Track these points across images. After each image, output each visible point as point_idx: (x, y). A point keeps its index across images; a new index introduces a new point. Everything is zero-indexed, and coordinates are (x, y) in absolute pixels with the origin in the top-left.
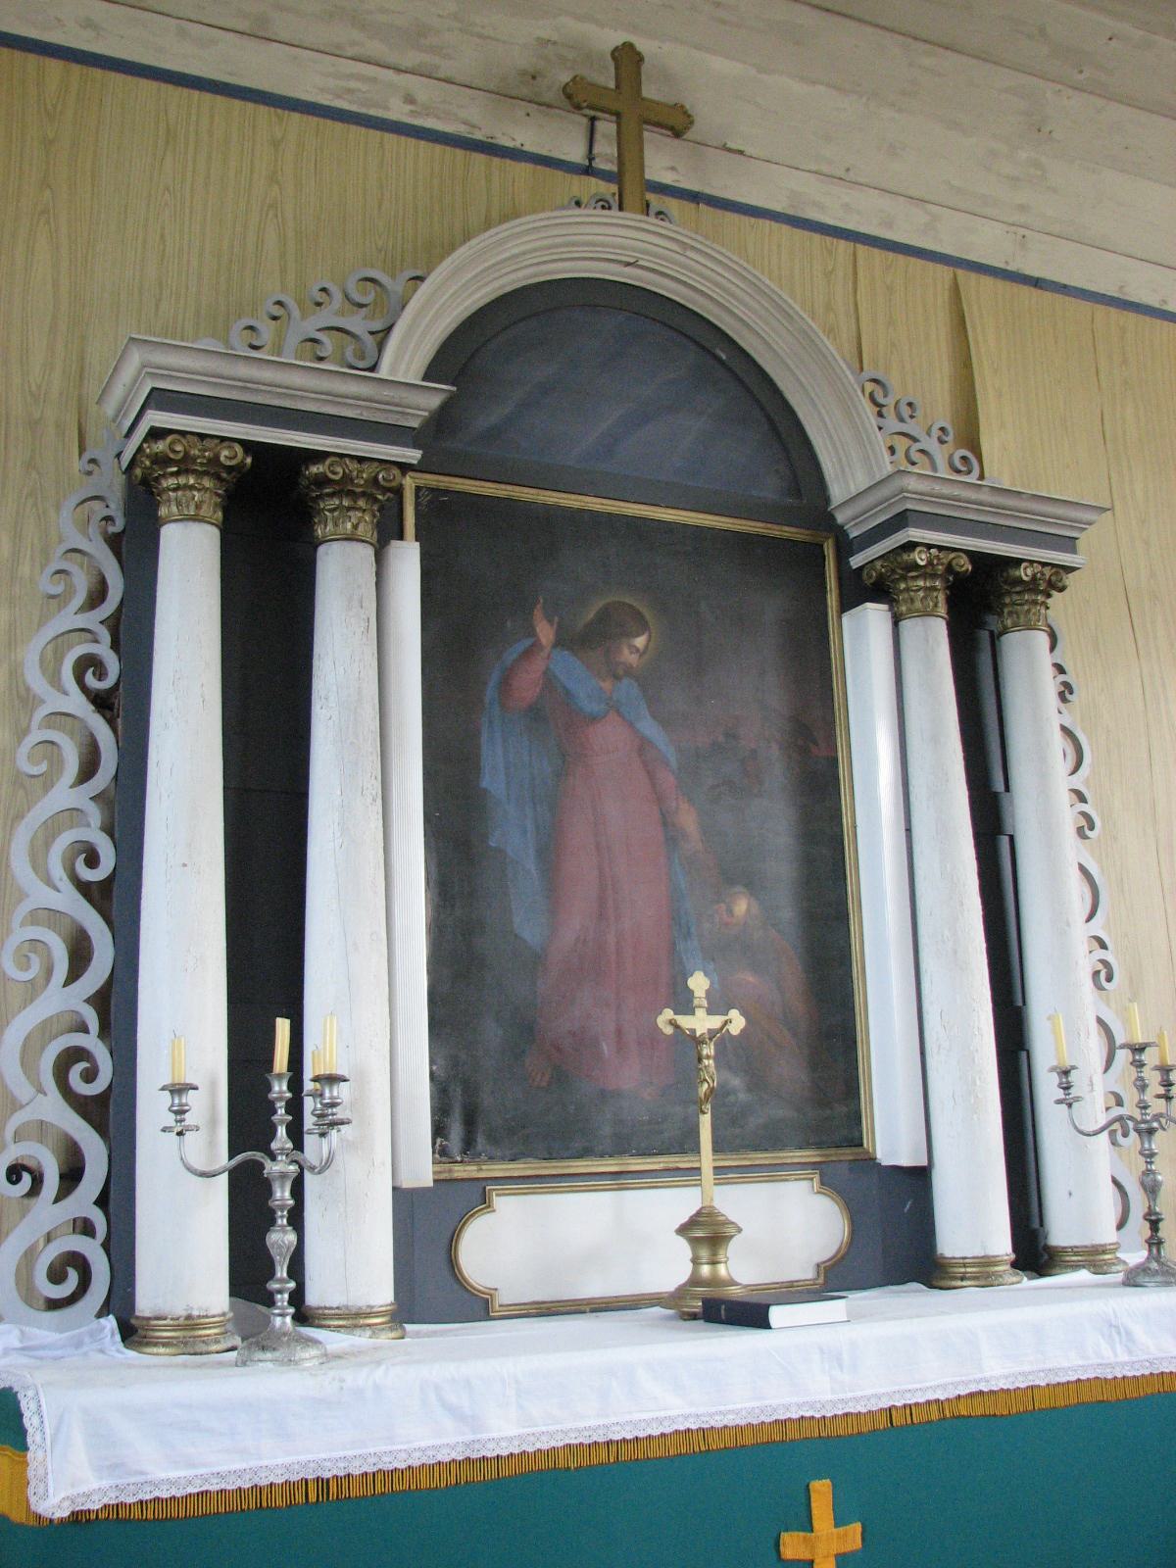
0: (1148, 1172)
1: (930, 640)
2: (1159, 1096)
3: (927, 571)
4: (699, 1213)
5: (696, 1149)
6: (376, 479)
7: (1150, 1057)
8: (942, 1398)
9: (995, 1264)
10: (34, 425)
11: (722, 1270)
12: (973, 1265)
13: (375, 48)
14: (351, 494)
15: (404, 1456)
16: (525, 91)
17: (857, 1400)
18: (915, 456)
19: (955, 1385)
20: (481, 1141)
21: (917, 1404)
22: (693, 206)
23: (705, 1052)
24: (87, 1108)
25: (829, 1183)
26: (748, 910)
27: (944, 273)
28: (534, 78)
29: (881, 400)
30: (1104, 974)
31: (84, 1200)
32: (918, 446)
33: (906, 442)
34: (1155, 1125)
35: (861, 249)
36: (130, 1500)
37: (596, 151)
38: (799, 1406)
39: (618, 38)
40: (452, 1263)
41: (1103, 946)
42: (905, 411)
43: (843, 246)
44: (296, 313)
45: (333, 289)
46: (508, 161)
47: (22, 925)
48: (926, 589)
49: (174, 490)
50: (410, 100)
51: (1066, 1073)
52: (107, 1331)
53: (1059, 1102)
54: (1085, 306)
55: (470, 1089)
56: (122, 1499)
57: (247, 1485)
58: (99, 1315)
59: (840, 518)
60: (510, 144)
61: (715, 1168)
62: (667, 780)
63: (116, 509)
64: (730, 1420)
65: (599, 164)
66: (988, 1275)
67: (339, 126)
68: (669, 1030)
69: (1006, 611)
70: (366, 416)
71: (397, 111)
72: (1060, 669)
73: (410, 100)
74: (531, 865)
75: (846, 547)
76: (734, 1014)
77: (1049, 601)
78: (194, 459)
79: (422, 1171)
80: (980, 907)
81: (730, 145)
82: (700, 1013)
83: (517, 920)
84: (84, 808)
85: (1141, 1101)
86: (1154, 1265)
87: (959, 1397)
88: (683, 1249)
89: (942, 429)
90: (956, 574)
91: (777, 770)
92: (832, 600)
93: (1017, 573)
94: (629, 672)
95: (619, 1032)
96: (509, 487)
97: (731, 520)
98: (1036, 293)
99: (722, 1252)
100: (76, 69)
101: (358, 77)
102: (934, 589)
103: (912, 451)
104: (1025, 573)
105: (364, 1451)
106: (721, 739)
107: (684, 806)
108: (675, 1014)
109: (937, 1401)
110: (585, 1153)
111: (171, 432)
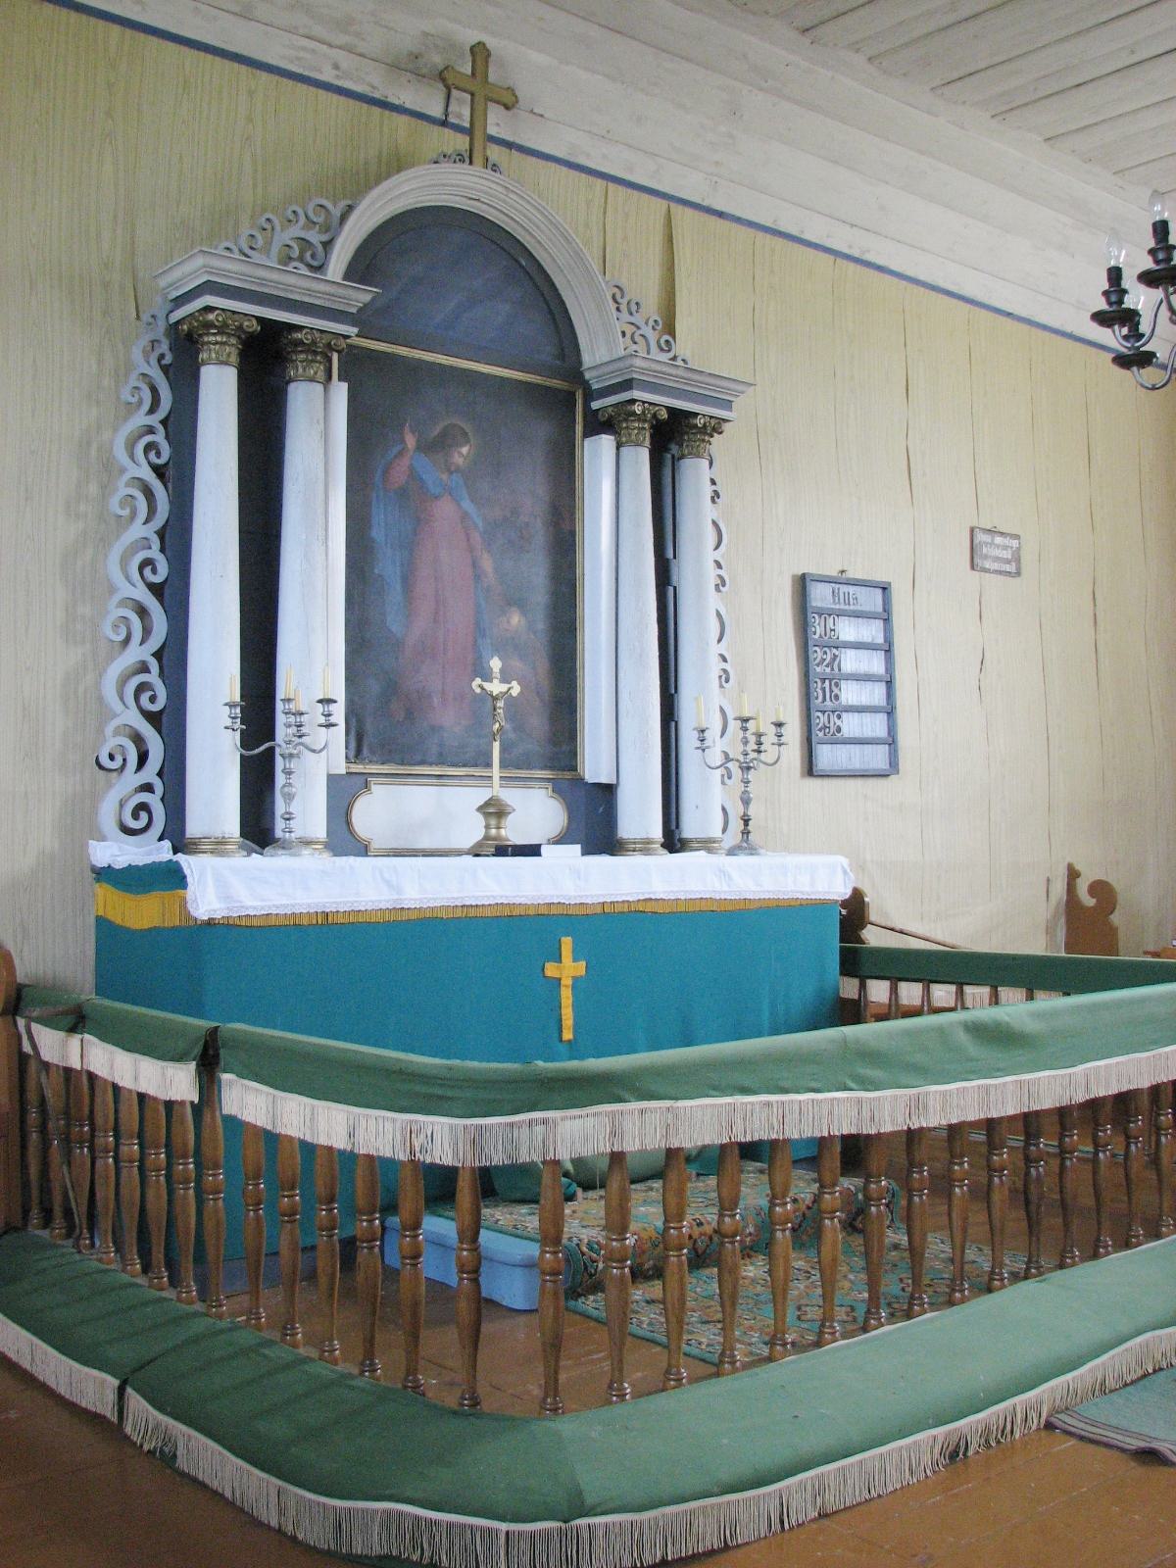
0: (745, 792)
1: (639, 459)
2: (754, 751)
3: (641, 418)
4: (490, 799)
5: (489, 765)
6: (330, 343)
7: (750, 725)
8: (631, 900)
9: (652, 843)
10: (106, 285)
11: (503, 832)
12: (639, 843)
13: (318, 30)
14: (315, 353)
15: (364, 904)
16: (410, 66)
17: (587, 896)
18: (637, 338)
19: (638, 893)
20: (365, 751)
21: (617, 902)
22: (508, 151)
23: (498, 705)
24: (153, 718)
25: (558, 790)
26: (519, 621)
27: (664, 204)
28: (416, 58)
29: (619, 300)
30: (725, 676)
31: (149, 774)
32: (641, 332)
33: (634, 329)
34: (751, 765)
35: (612, 186)
36: (235, 915)
37: (450, 109)
38: (558, 897)
39: (473, 36)
40: (348, 823)
41: (725, 660)
42: (634, 308)
43: (600, 183)
44: (278, 228)
45: (300, 211)
46: (394, 114)
47: (117, 607)
48: (639, 428)
49: (213, 344)
50: (336, 67)
51: (703, 731)
52: (166, 848)
53: (698, 748)
54: (751, 231)
55: (360, 722)
56: (231, 914)
57: (290, 912)
58: (160, 839)
59: (587, 376)
60: (397, 102)
61: (501, 777)
62: (476, 537)
63: (164, 347)
64: (523, 901)
65: (452, 119)
66: (649, 849)
67: (290, 83)
68: (478, 691)
69: (685, 445)
70: (327, 304)
71: (327, 75)
72: (713, 482)
73: (336, 67)
74: (398, 587)
75: (589, 395)
76: (514, 683)
77: (711, 439)
78: (228, 326)
79: (341, 768)
80: (657, 630)
81: (535, 111)
82: (496, 681)
83: (389, 618)
84: (148, 537)
85: (745, 751)
86: (745, 845)
87: (639, 901)
88: (480, 819)
89: (656, 321)
90: (657, 420)
91: (540, 536)
92: (579, 428)
93: (695, 422)
94: (458, 470)
95: (443, 692)
96: (394, 346)
97: (521, 374)
98: (720, 221)
99: (503, 822)
100: (129, 32)
101: (304, 49)
102: (645, 428)
103: (636, 335)
104: (699, 422)
105: (345, 899)
106: (509, 515)
107: (485, 555)
108: (482, 680)
109: (628, 901)
110: (422, 763)
111: (217, 308)
